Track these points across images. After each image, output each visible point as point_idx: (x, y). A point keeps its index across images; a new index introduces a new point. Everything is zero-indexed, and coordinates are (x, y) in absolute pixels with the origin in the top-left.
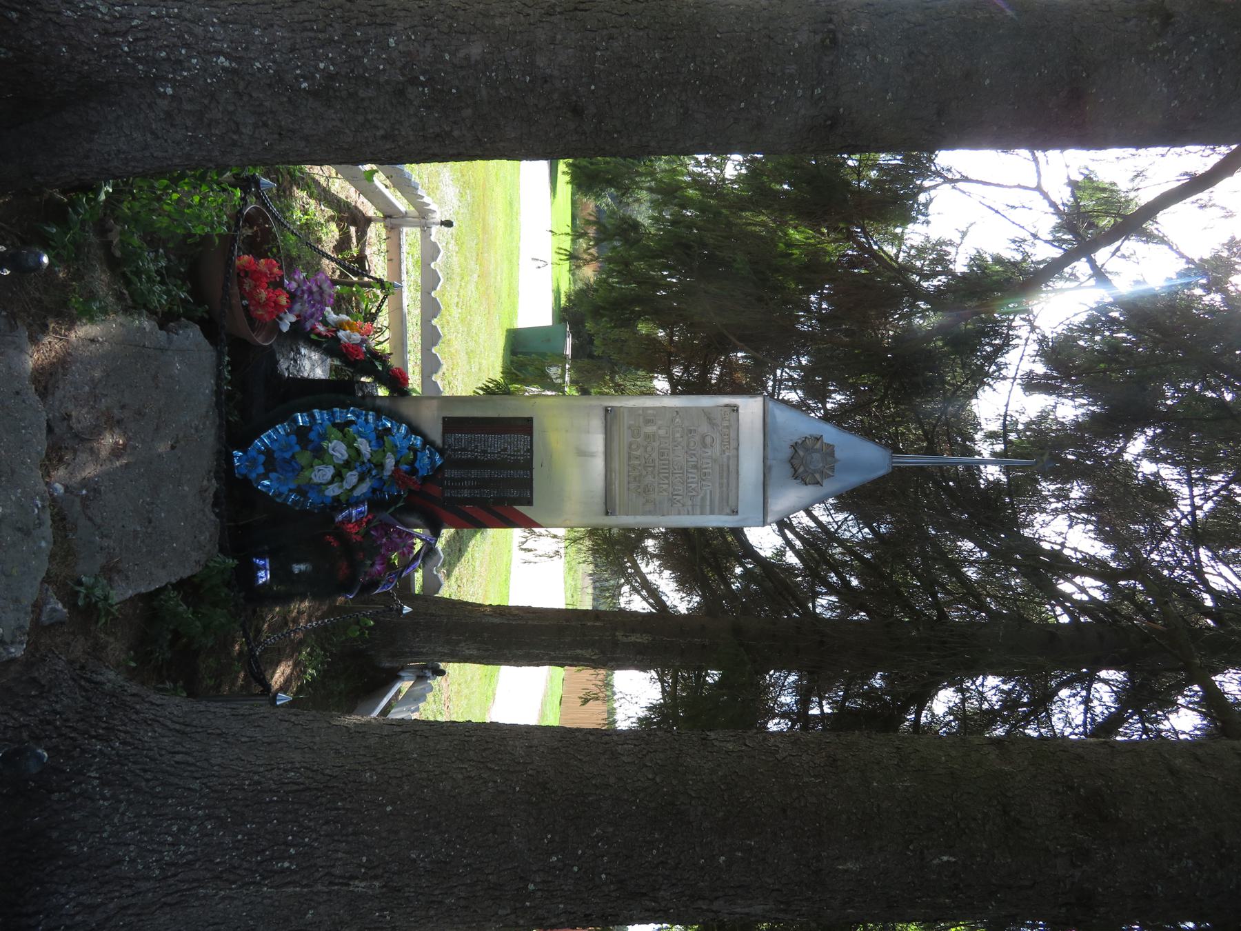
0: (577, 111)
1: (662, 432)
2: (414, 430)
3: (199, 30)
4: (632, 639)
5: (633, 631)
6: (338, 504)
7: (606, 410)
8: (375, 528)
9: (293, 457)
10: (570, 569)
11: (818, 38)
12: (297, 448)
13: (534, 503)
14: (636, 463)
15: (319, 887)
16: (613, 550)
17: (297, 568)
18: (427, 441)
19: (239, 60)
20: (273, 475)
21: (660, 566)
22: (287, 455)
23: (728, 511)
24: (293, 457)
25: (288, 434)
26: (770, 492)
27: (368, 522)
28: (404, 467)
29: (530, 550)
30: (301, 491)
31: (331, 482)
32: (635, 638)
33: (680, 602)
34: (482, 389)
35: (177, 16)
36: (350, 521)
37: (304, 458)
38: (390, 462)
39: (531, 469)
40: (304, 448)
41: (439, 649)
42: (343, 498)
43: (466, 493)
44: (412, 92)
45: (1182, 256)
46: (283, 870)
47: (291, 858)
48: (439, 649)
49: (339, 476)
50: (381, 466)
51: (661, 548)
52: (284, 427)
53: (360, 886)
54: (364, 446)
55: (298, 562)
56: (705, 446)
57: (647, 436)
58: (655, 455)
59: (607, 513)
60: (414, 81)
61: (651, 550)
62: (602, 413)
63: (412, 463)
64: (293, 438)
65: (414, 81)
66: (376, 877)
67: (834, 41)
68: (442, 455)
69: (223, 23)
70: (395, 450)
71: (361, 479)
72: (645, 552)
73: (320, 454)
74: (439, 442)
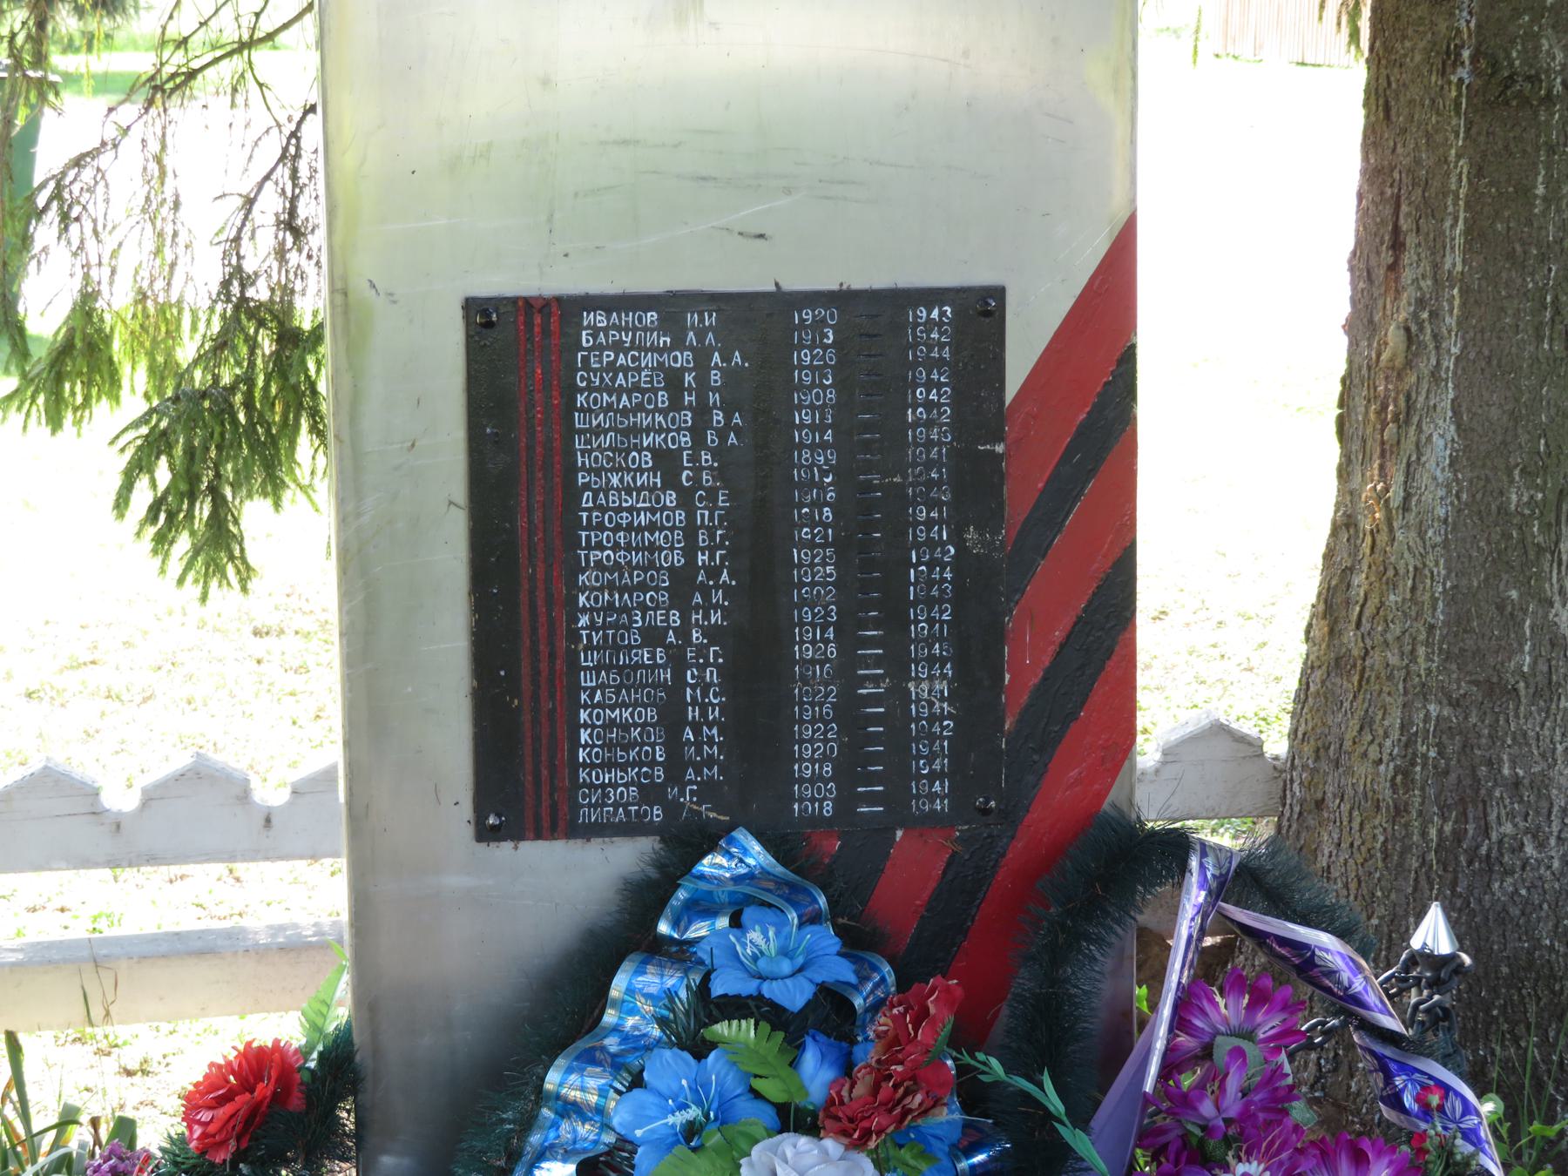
13: (980, 276)
18: (630, 931)
28: (815, 1074)
39: (782, 303)
68: (711, 839)
74: (626, 857)
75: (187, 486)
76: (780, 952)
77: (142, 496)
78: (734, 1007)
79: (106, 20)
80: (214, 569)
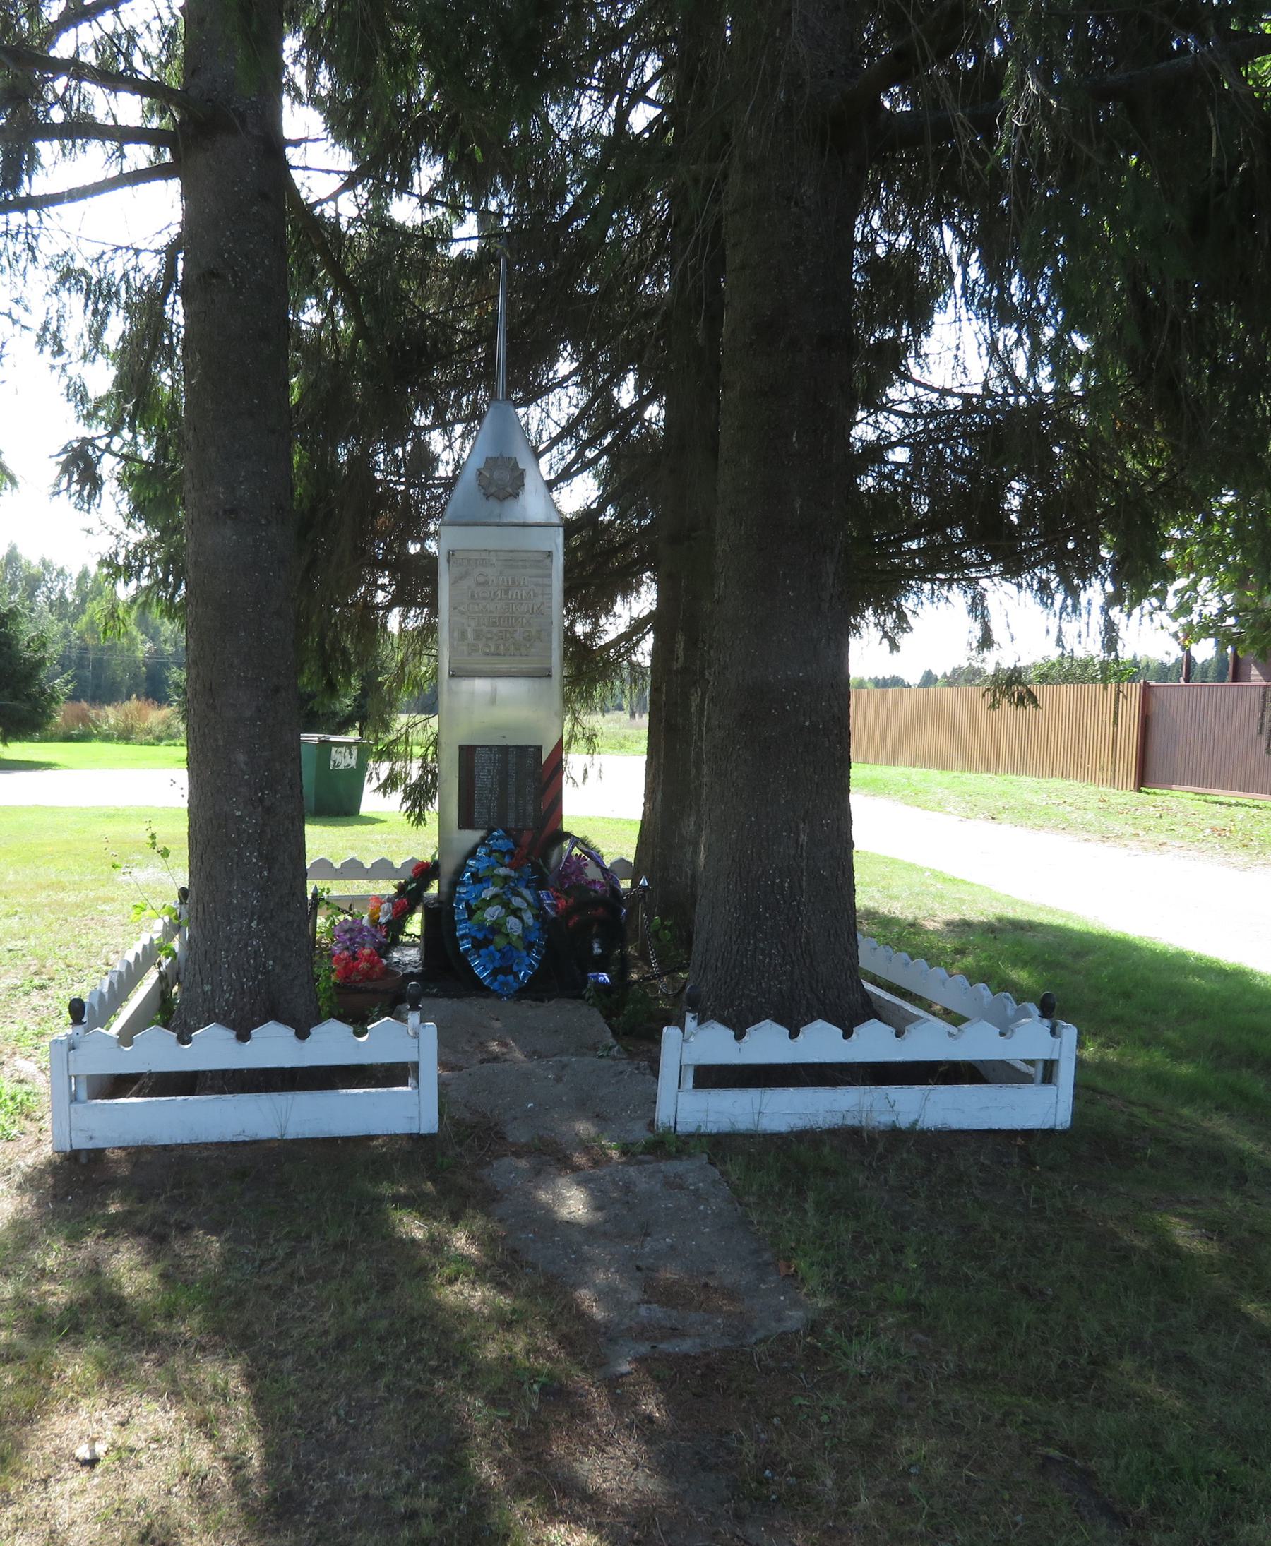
0: (277, 690)
1: (473, 623)
2: (472, 854)
3: (235, 938)
4: (680, 652)
5: (672, 651)
6: (540, 916)
7: (452, 676)
8: (562, 886)
9: (499, 951)
10: (622, 746)
11: (229, 522)
12: (491, 948)
13: (538, 744)
14: (501, 650)
15: (804, 864)
16: (588, 670)
17: (597, 950)
18: (483, 842)
19: (253, 914)
20: (515, 969)
21: (607, 614)
22: (498, 955)
23: (548, 561)
24: (499, 951)
25: (479, 956)
26: (530, 521)
27: (557, 891)
28: (507, 860)
29: (586, 771)
30: (529, 946)
31: (521, 919)
32: (680, 649)
33: (644, 601)
34: (409, 817)
35: (227, 951)
36: (556, 906)
37: (500, 942)
38: (502, 871)
39: (507, 747)
40: (491, 942)
41: (689, 856)
42: (536, 912)
43: (530, 808)
44: (267, 803)
45: (338, 173)
46: (790, 887)
47: (782, 882)
48: (689, 856)
49: (516, 912)
50: (506, 879)
51: (586, 616)
52: (474, 960)
53: (803, 838)
54: (488, 893)
55: (592, 948)
56: (485, 583)
57: (477, 638)
58: (495, 630)
59: (550, 676)
60: (261, 800)
61: (588, 629)
62: (455, 680)
63: (503, 854)
64: (483, 951)
65: (261, 800)
66: (797, 827)
67: (232, 511)
68: (494, 830)
69: (230, 923)
70: (490, 868)
71: (519, 895)
72: (590, 636)
73: (497, 928)
74: (481, 833)
75: (414, 805)
76: (503, 844)
77: (404, 807)
78: (495, 851)
79: (427, 212)
80: (419, 823)
